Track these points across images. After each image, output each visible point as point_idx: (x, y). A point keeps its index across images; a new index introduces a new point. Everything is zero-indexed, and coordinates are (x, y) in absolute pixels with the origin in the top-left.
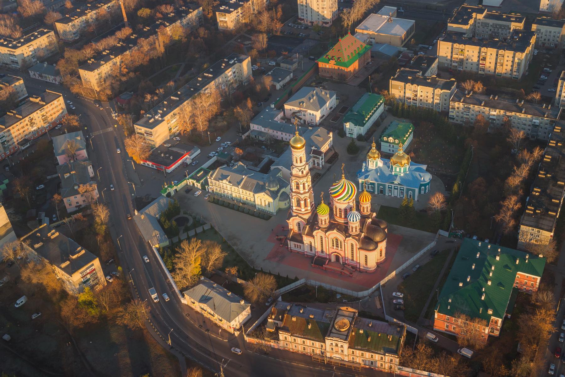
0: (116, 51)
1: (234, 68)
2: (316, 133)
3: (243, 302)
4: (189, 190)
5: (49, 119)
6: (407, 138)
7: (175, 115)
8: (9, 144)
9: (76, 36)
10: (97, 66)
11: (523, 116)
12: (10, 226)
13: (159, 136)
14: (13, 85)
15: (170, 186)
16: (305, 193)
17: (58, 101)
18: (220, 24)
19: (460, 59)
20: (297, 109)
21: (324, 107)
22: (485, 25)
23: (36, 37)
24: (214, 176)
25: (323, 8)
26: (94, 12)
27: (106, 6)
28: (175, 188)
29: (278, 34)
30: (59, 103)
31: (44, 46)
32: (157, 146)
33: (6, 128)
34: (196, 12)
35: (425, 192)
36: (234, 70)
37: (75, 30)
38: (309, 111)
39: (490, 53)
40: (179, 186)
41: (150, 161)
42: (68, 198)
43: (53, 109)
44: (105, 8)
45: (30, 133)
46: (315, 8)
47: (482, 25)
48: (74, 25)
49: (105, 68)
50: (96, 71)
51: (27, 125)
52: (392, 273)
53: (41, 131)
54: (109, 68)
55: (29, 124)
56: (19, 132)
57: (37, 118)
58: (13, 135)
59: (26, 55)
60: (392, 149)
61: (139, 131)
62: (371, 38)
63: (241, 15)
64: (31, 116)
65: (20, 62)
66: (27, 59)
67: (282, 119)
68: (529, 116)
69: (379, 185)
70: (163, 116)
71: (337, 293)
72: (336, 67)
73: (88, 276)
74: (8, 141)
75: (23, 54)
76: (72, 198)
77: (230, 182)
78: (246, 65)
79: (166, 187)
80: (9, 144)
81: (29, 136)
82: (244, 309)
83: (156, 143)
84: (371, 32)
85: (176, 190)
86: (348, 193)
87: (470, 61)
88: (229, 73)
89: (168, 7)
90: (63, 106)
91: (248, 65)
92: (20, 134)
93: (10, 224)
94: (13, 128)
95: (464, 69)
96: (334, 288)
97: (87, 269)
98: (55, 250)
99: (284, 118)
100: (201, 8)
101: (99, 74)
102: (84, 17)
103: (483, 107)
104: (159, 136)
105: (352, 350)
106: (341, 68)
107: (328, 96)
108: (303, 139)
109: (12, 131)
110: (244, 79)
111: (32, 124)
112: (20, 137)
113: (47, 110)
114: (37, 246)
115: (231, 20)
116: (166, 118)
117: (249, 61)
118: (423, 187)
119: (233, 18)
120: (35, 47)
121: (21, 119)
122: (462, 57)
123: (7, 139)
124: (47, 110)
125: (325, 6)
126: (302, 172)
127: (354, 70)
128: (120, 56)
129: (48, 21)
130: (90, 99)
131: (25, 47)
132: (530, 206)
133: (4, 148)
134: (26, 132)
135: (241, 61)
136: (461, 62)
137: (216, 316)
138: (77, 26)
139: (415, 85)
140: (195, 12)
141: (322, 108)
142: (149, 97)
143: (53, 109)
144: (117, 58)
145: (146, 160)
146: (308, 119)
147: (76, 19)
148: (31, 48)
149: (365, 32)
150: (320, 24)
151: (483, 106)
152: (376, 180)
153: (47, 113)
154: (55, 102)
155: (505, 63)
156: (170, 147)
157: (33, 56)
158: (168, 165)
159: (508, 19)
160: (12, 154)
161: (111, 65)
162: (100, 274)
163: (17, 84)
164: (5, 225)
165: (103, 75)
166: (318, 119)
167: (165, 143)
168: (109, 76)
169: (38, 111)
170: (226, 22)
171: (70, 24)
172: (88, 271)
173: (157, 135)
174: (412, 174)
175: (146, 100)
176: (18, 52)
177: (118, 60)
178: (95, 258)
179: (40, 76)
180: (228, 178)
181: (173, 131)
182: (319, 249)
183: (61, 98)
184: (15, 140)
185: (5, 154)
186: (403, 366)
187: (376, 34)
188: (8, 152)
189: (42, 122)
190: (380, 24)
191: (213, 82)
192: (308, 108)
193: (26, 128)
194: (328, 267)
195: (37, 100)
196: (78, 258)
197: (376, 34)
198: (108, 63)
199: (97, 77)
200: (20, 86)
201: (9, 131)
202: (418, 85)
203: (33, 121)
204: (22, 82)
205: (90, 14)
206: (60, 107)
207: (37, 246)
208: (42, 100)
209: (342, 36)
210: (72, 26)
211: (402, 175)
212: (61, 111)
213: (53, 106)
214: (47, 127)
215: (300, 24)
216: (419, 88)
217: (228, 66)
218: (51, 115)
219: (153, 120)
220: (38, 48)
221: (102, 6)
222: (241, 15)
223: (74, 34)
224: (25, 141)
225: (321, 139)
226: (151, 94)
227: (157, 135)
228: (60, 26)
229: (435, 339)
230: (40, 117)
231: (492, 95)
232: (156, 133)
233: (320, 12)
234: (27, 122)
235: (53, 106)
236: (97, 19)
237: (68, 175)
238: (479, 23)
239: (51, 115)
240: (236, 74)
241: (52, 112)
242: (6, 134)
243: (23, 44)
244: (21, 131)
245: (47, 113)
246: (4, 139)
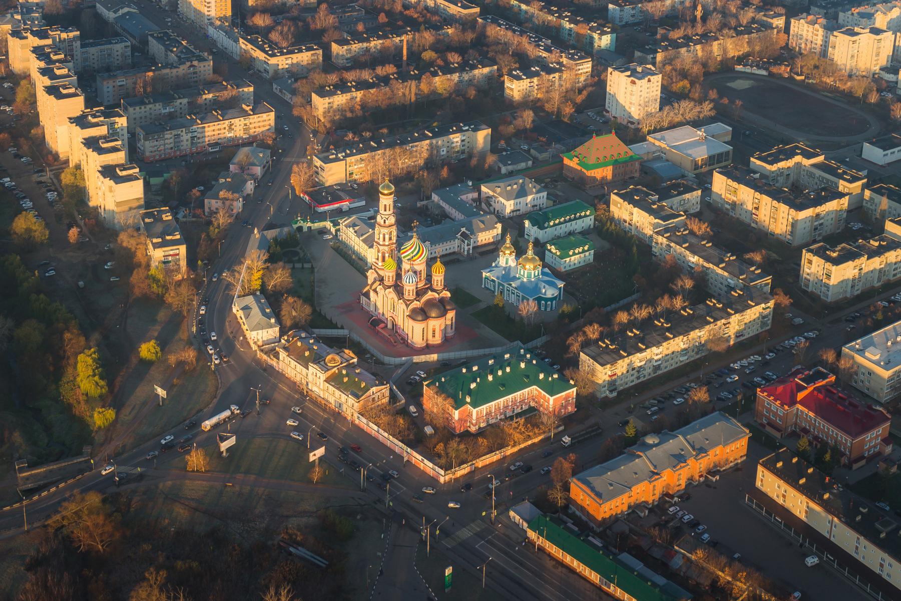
0: (362, 85)
1: (464, 136)
2: (481, 219)
3: (273, 321)
4: (323, 231)
5: (252, 131)
6: (574, 254)
7: (362, 160)
8: (199, 141)
9: (348, 63)
10: (331, 94)
11: (720, 271)
12: (142, 202)
13: (332, 175)
14: (241, 90)
15: (305, 220)
16: (384, 245)
17: (267, 116)
18: (507, 91)
19: (733, 201)
20: (491, 193)
21: (521, 200)
22: (811, 175)
23: (300, 51)
24: (346, 222)
25: (631, 103)
26: (381, 41)
27: (399, 38)
28: (309, 224)
29: (566, 120)
30: (268, 118)
31: (305, 63)
32: (327, 184)
33: (202, 124)
34: (486, 70)
35: (546, 309)
36: (464, 138)
37: (349, 56)
38: (501, 199)
39: (766, 201)
40: (316, 224)
41: (308, 195)
42: (209, 200)
43: (259, 122)
44: (397, 41)
45: (225, 138)
46: (621, 100)
47: (807, 175)
48: (350, 49)
49: (340, 100)
50: (327, 98)
51: (225, 128)
52: (432, 355)
53: (238, 140)
54: (344, 101)
55: (227, 128)
56: (213, 133)
57: (238, 125)
58: (207, 134)
59: (280, 67)
60: (554, 262)
61: (316, 164)
62: (662, 152)
63: (536, 87)
64: (233, 121)
65: (271, 72)
66: (280, 72)
67: (474, 200)
68: (726, 274)
69: (500, 284)
70: (347, 156)
71: (369, 352)
72: (579, 168)
73: (170, 258)
74: (199, 138)
75: (278, 65)
76: (213, 201)
77: (355, 232)
78: (482, 136)
79: (299, 218)
80: (199, 141)
81: (222, 141)
82: (271, 326)
83: (327, 181)
84: (663, 146)
85: (310, 227)
86: (412, 252)
87: (745, 207)
88: (456, 139)
89: (456, 56)
90: (272, 123)
91: (485, 138)
92: (214, 135)
93: (143, 200)
94: (209, 126)
95: (738, 216)
96: (369, 347)
97: (172, 250)
98: (159, 228)
99: (478, 200)
100: (496, 67)
101: (329, 103)
102: (365, 45)
103: (683, 250)
104: (332, 175)
105: (328, 385)
106: (583, 170)
107: (534, 190)
108: (393, 186)
109: (207, 129)
110: (475, 151)
111: (230, 128)
112: (213, 138)
113: (251, 121)
114: (147, 220)
115: (519, 88)
116: (348, 159)
117: (488, 134)
118: (549, 303)
119: (521, 88)
120: (295, 61)
121: (221, 121)
122: (735, 199)
123: (199, 135)
124: (251, 121)
125: (633, 102)
126: (385, 222)
127: (603, 178)
128: (362, 92)
129: (325, 39)
130: (312, 126)
131: (283, 57)
132: (607, 339)
133: (192, 143)
134: (222, 136)
135: (476, 130)
136: (734, 205)
137: (246, 326)
138: (352, 51)
139: (631, 205)
140: (484, 69)
141: (518, 200)
142: (351, 136)
143: (259, 122)
144: (358, 92)
145: (305, 193)
146: (497, 207)
147: (355, 43)
148: (289, 62)
149: (657, 143)
150: (625, 123)
151: (684, 248)
152: (498, 278)
153: (250, 123)
154: (264, 115)
155: (781, 220)
156: (337, 190)
157: (288, 71)
158: (322, 203)
159: (841, 177)
160: (198, 153)
161: (349, 97)
162: (183, 263)
163: (246, 89)
164: (138, 199)
165: (335, 106)
166: (508, 210)
167: (336, 185)
168: (341, 110)
169: (242, 119)
170: (512, 90)
171: (345, 47)
172: (171, 253)
173: (330, 173)
174: (537, 284)
175: (346, 138)
176: (273, 61)
177: (359, 95)
178: (183, 244)
179: (281, 91)
180: (356, 228)
181: (355, 177)
182: (381, 311)
183: (272, 115)
184: (207, 139)
185: (191, 149)
186: (362, 415)
187: (668, 148)
188: (194, 149)
189: (242, 132)
190: (685, 140)
191: (428, 142)
192: (500, 194)
193: (223, 131)
194: (381, 330)
195: (247, 109)
196: (171, 240)
197: (668, 148)
198: (344, 95)
199: (326, 106)
200: (249, 93)
201: (204, 127)
202: (634, 207)
203: (233, 127)
204: (251, 89)
205: (375, 42)
206: (267, 123)
207: (147, 220)
208: (252, 110)
209: (597, 135)
210: (347, 50)
211: (525, 280)
212: (268, 127)
213: (260, 119)
214: (245, 138)
215: (604, 116)
216: (636, 211)
217: (460, 130)
218: (255, 128)
219: (334, 156)
220: (298, 64)
221: (393, 37)
222: (536, 87)
223: (347, 59)
224: (216, 144)
225: (482, 226)
226: (354, 133)
227: (330, 173)
228: (335, 47)
229: (414, 413)
230: (243, 125)
231: (78, 33)
232: (329, 171)
233: (627, 108)
234: (225, 126)
235: (260, 119)
236: (380, 51)
237: (224, 180)
238: (804, 170)
239: (255, 128)
240: (466, 143)
241: (257, 125)
242: (200, 130)
243: (282, 54)
244: (216, 132)
245: (250, 123)
246: (195, 134)
